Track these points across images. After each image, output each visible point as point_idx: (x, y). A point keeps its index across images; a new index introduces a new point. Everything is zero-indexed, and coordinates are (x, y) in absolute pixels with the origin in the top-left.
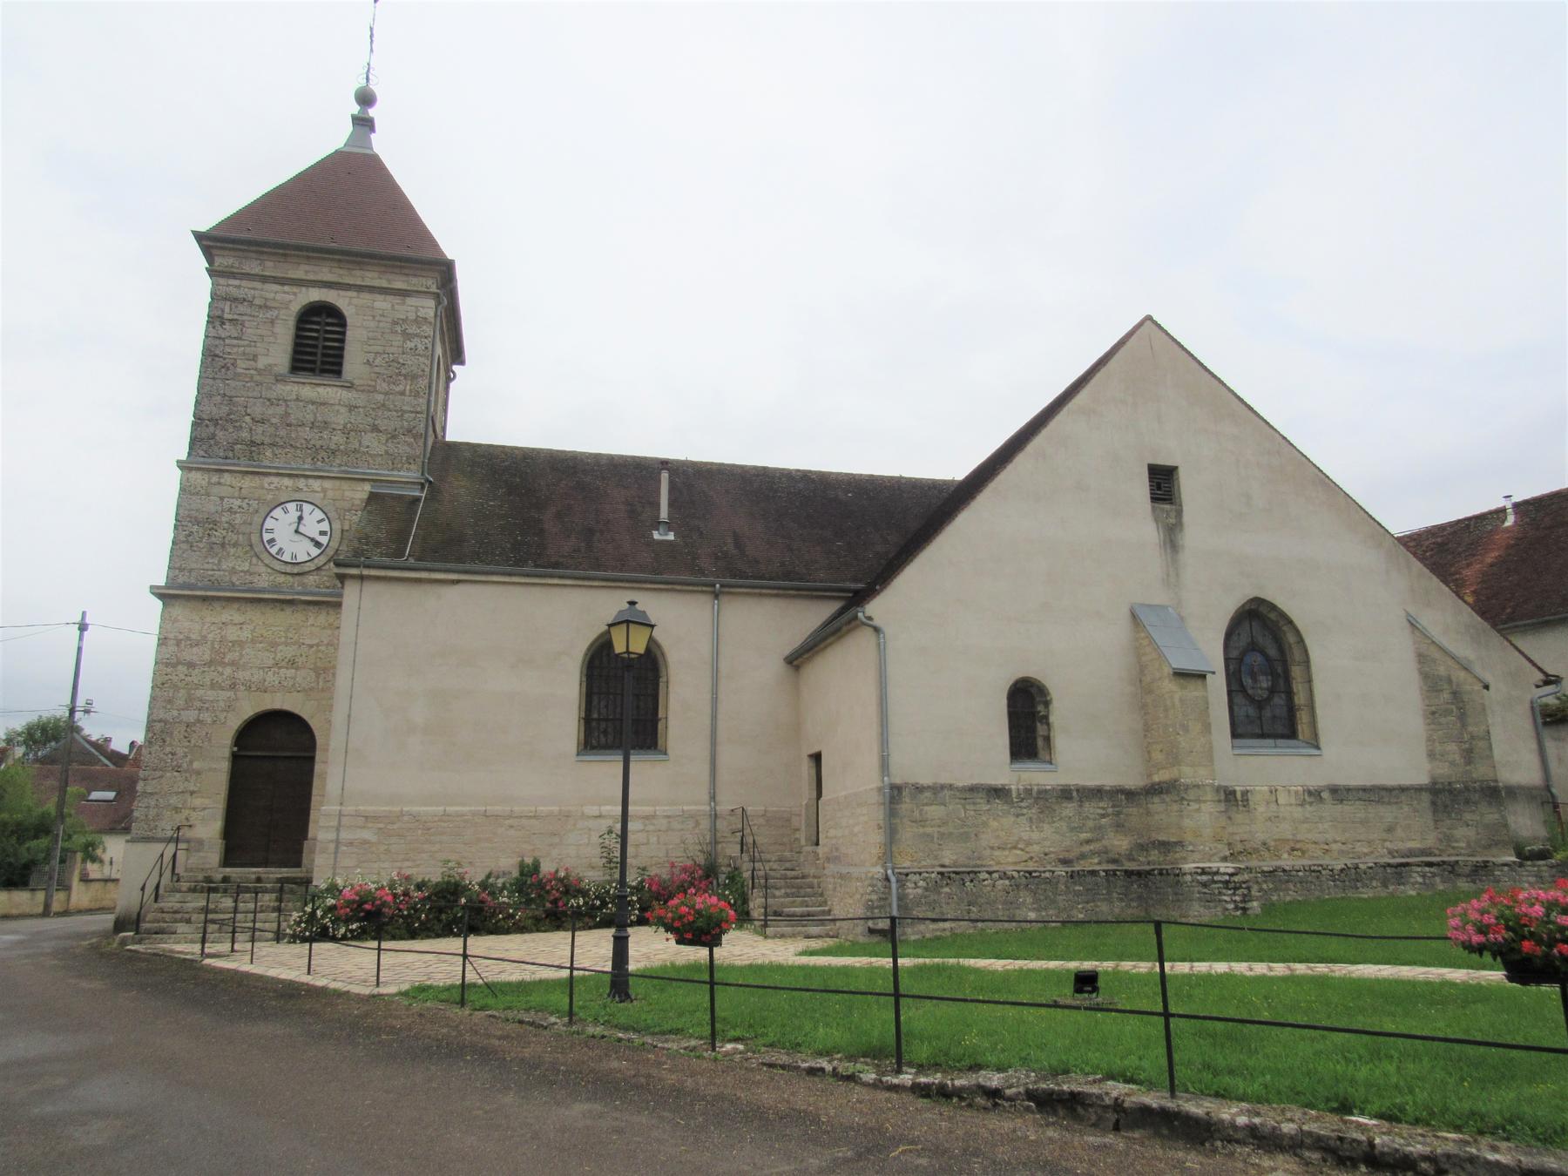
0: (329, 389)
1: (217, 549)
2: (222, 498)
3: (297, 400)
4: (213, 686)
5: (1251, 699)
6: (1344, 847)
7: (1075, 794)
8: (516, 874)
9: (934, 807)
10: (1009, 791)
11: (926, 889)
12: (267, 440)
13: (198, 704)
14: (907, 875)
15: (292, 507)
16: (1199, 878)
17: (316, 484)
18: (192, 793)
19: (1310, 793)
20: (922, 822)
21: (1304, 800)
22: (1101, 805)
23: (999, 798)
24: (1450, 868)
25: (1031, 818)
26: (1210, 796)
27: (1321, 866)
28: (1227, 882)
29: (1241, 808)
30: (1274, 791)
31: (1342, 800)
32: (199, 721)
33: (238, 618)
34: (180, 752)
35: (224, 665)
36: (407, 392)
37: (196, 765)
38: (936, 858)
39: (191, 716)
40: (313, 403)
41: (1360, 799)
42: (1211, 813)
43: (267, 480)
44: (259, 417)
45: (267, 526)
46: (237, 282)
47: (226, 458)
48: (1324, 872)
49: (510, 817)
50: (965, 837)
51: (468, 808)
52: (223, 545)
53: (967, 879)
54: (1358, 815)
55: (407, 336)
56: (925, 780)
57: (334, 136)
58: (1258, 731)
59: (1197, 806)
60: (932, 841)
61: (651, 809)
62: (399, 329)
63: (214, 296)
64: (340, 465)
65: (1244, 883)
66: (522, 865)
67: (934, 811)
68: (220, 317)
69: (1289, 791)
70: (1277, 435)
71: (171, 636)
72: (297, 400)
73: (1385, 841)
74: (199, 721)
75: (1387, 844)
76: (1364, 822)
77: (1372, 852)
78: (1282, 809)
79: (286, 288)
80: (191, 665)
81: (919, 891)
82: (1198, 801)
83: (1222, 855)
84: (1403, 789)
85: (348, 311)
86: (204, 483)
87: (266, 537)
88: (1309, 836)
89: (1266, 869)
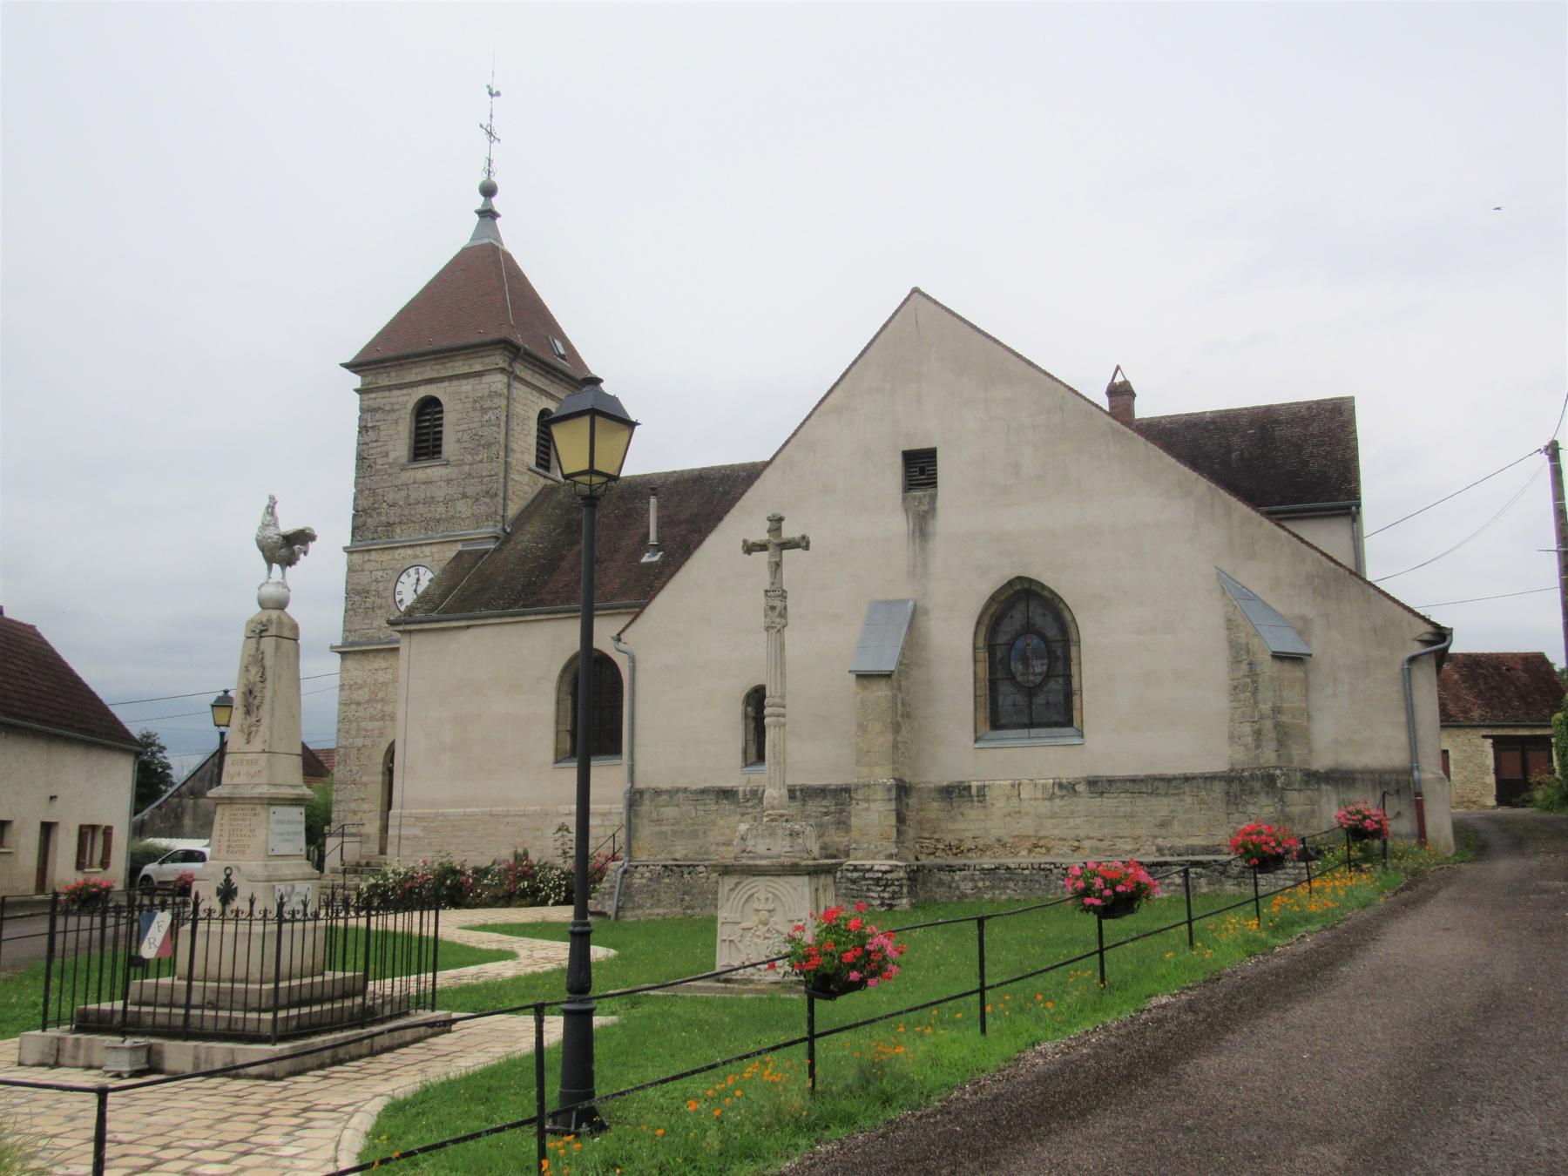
0: (434, 469)
1: (370, 613)
2: (371, 572)
3: (415, 483)
4: (372, 718)
5: (1020, 687)
6: (1101, 845)
7: (798, 794)
8: (512, 861)
9: (669, 809)
10: (737, 792)
11: (650, 880)
12: (397, 520)
13: (363, 733)
14: (637, 867)
15: (412, 571)
16: (849, 874)
17: (427, 550)
18: (363, 799)
19: (1061, 786)
20: (659, 822)
21: (1053, 793)
22: (824, 803)
23: (726, 798)
24: (1221, 868)
25: (755, 817)
26: (880, 794)
27: (1054, 864)
28: (879, 879)
29: (976, 804)
30: (1017, 786)
31: (1102, 793)
32: (364, 746)
33: (384, 664)
34: (355, 769)
35: (377, 701)
36: (485, 460)
37: (364, 779)
38: (669, 852)
39: (359, 742)
40: (424, 483)
41: (1127, 791)
42: (880, 812)
43: (398, 552)
44: (391, 502)
45: (398, 589)
46: (373, 395)
47: (374, 539)
48: (1055, 871)
49: (508, 816)
50: (694, 834)
51: (479, 809)
52: (373, 609)
53: (686, 871)
54: (1122, 809)
55: (484, 410)
56: (665, 785)
57: (460, 234)
58: (1026, 720)
59: (865, 805)
60: (666, 838)
61: (608, 806)
62: (478, 406)
63: (362, 410)
64: (443, 531)
65: (898, 880)
66: (516, 855)
67: (670, 812)
68: (365, 427)
69: (1036, 785)
70: (1062, 387)
71: (346, 683)
72: (415, 483)
73: (1156, 837)
74: (364, 746)
75: (1159, 841)
76: (1131, 816)
77: (1138, 850)
78: (1025, 804)
79: (405, 391)
80: (358, 704)
81: (644, 881)
82: (867, 800)
83: (888, 853)
84: (1187, 779)
85: (443, 399)
86: (361, 562)
87: (398, 598)
88: (1055, 832)
89: (986, 866)
